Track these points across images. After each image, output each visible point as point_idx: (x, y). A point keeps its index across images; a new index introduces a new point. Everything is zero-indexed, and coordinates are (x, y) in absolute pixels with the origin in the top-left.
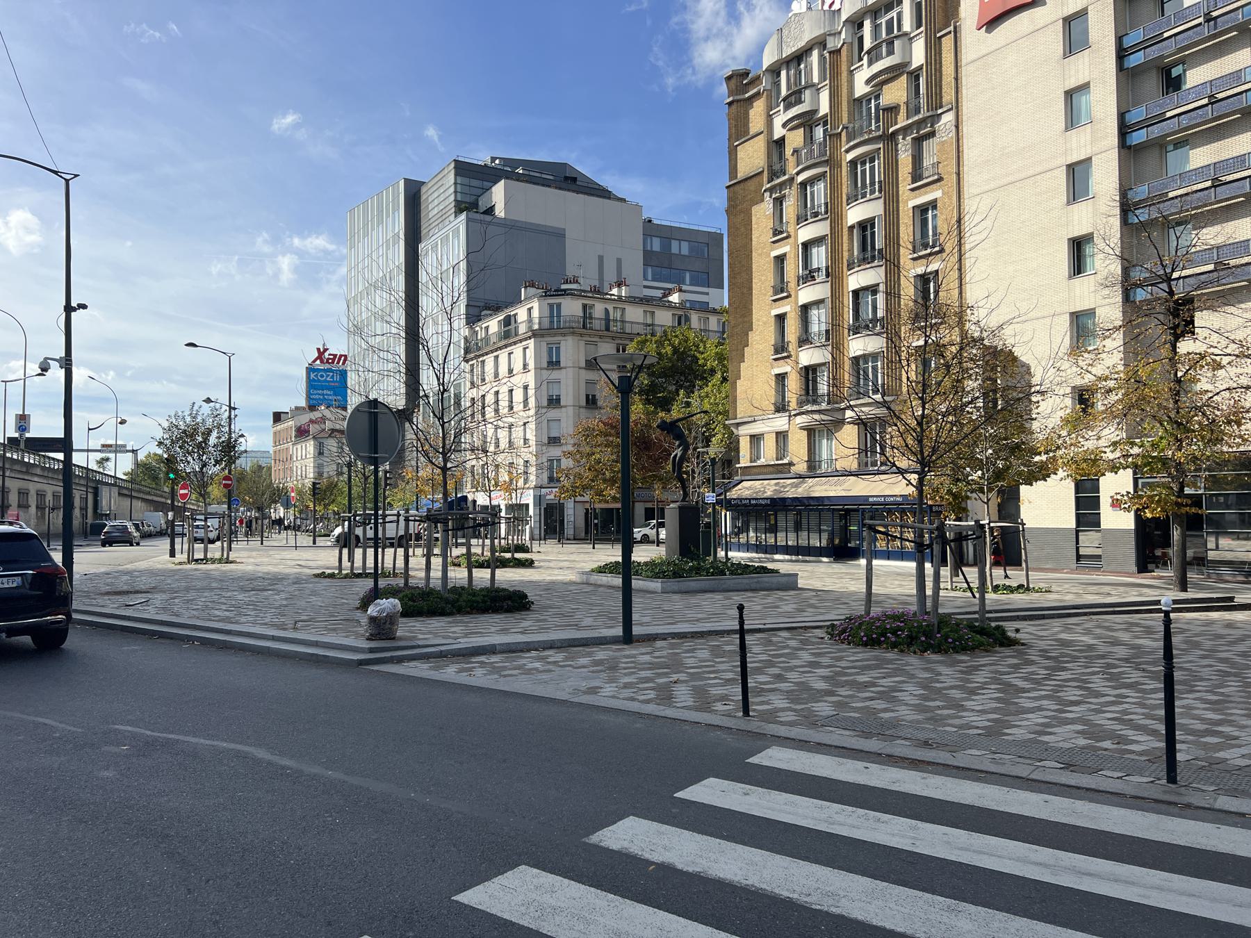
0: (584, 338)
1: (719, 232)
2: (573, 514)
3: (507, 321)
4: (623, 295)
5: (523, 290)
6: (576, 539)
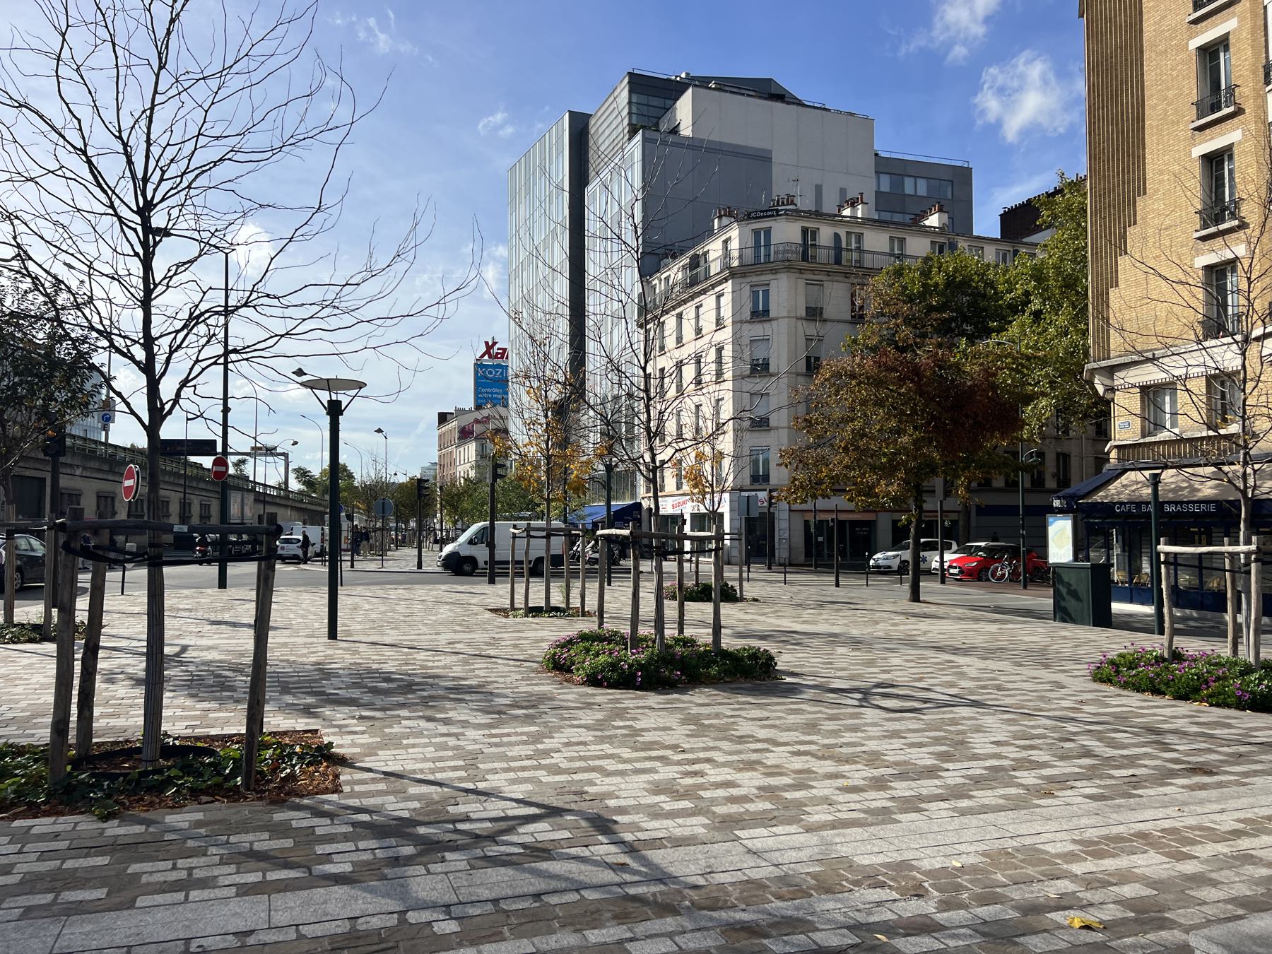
0: (805, 276)
1: (966, 165)
2: (787, 530)
3: (695, 263)
4: (859, 215)
5: (716, 221)
6: (791, 565)
